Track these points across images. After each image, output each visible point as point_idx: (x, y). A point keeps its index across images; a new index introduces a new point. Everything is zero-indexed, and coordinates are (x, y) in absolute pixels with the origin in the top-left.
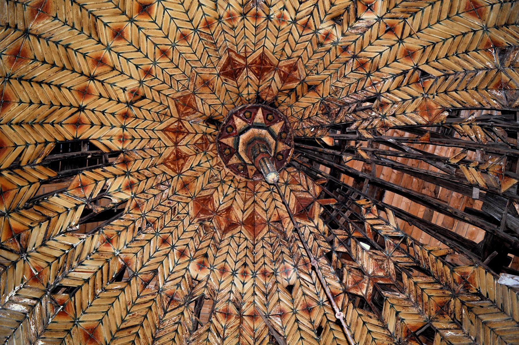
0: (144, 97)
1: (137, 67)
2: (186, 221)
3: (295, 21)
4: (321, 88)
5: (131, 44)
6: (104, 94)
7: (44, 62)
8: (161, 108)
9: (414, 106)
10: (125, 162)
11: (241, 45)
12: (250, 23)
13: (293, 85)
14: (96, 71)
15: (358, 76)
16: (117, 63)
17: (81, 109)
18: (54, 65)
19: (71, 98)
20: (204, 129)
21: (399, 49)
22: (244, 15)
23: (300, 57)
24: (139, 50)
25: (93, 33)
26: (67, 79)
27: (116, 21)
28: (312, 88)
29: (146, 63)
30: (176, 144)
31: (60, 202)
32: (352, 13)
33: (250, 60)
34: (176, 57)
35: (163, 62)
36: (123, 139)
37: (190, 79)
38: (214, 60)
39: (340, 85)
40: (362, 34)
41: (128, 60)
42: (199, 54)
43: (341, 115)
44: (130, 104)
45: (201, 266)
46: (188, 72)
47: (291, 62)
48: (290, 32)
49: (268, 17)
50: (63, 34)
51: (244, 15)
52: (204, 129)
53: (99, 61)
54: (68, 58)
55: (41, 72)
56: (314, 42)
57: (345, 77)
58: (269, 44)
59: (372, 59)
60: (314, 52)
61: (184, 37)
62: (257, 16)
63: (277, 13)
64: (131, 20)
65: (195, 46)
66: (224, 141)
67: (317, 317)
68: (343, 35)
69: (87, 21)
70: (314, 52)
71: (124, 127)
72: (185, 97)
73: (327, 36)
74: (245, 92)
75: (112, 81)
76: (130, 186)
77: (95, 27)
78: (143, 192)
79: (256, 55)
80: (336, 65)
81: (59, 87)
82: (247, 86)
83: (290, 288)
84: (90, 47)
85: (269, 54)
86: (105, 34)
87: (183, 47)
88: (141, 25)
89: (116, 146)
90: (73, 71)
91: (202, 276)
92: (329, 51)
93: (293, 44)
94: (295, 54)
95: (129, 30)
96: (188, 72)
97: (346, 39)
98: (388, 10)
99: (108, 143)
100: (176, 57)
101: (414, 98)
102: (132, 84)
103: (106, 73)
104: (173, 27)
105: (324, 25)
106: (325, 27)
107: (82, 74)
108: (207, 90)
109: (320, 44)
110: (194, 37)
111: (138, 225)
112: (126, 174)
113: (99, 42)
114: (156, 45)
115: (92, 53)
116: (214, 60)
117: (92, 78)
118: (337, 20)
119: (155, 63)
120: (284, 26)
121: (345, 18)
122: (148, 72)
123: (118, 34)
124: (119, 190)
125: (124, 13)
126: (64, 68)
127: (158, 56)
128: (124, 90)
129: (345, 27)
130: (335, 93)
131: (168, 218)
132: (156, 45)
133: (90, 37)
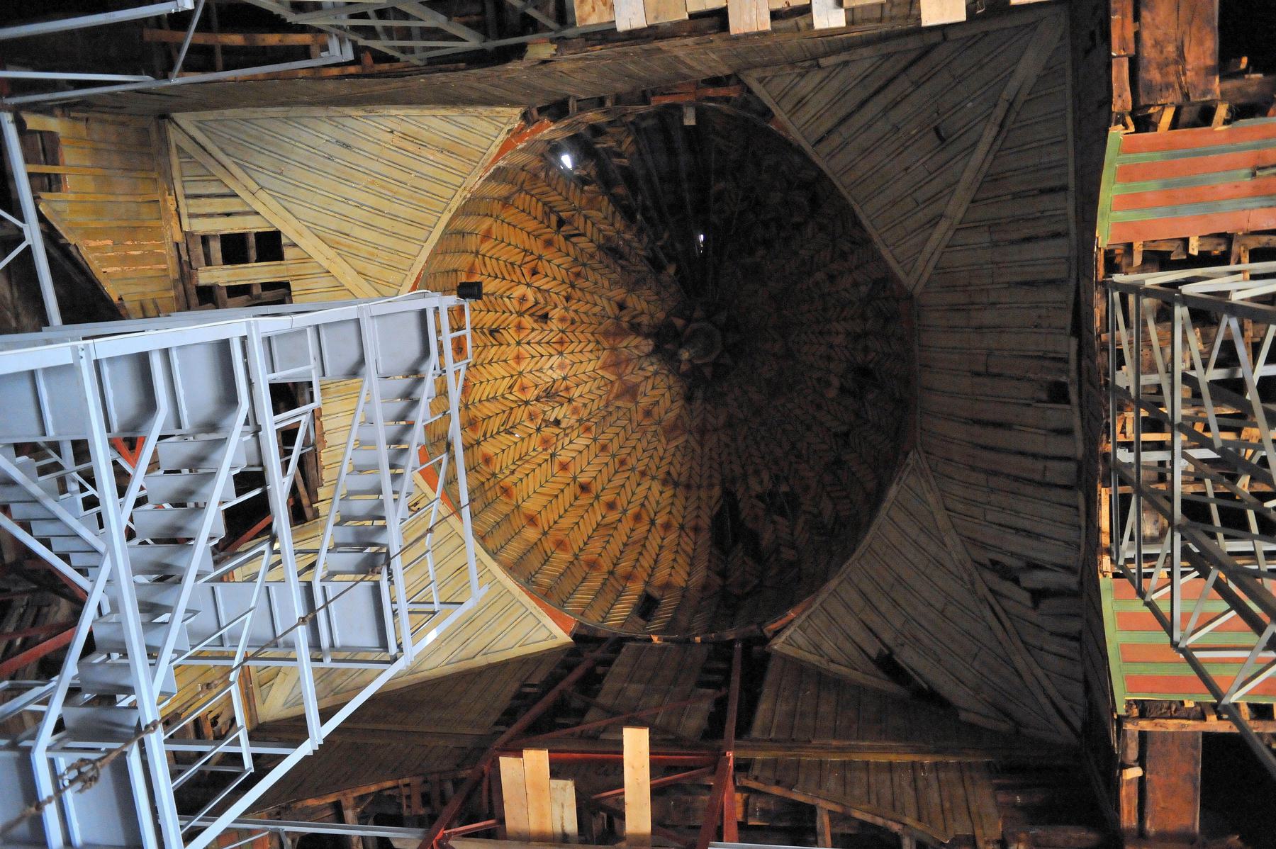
0: (668, 473)
1: (639, 485)
2: (789, 406)
3: (561, 353)
4: (618, 298)
5: (618, 494)
6: (668, 510)
7: (638, 560)
8: (678, 454)
9: (593, 213)
10: (733, 481)
11: (600, 392)
12: (576, 393)
13: (559, 413)
14: (646, 519)
15: (590, 272)
16: (639, 502)
17: (682, 527)
18: (641, 554)
19: (672, 536)
20: (699, 402)
21: (547, 254)
22: (570, 400)
23: (593, 334)
24: (623, 486)
25: (614, 526)
26: (654, 542)
27: (599, 509)
28: (622, 306)
29: (635, 477)
30: (716, 430)
31: (767, 538)
32: (534, 310)
33: (613, 378)
34: (625, 451)
35: (632, 461)
36: (711, 486)
37: (645, 432)
38: (621, 414)
39: (606, 284)
40: (548, 291)
41: (633, 494)
42: (618, 430)
43: (639, 268)
44: (676, 485)
45: (828, 384)
46: (638, 436)
47: (601, 339)
48: (572, 353)
49: (564, 379)
50: (614, 547)
51: (570, 400)
52: (699, 402)
53: (637, 518)
54: (635, 543)
55: (646, 562)
56: (572, 328)
57: (596, 283)
58: (591, 367)
59: (567, 270)
60: (583, 322)
61: (604, 448)
62: (567, 389)
63: (558, 372)
64: (597, 497)
65: (611, 436)
66: (709, 377)
67: (846, 247)
68: (556, 306)
69: (602, 531)
70: (583, 322)
71: (699, 487)
72: (665, 432)
73: (562, 320)
74: (651, 369)
75: (654, 505)
76: (757, 472)
77: (606, 525)
78: (763, 458)
79: (607, 375)
80: (588, 297)
81: (661, 547)
82: (643, 369)
83: (831, 278)
84: (625, 528)
85: (600, 363)
86: (613, 516)
87: (614, 447)
88: (600, 488)
89: (717, 491)
90: (647, 538)
91: (836, 382)
92: (576, 311)
93: (582, 345)
94: (592, 338)
95: (607, 497)
96: (638, 436)
97: (558, 302)
98: (520, 283)
99: (714, 501)
100: (625, 451)
101: (586, 218)
102: (656, 487)
103: (648, 512)
104: (597, 461)
105: (554, 328)
106: (554, 325)
107: (649, 531)
108: (656, 409)
109: (573, 322)
110: (603, 439)
111: (793, 459)
112: (745, 475)
113: (620, 520)
114: (616, 472)
115: (631, 524)
116: (621, 414)
117: (652, 522)
118: (545, 318)
119: (633, 469)
120: (568, 361)
121: (540, 313)
122: (643, 474)
123: (611, 506)
124: (761, 482)
125: (592, 505)
126: (644, 546)
127: (625, 467)
128: (661, 493)
129: (548, 308)
130: (616, 283)
131: (788, 427)
132: (616, 472)
133: (615, 528)
